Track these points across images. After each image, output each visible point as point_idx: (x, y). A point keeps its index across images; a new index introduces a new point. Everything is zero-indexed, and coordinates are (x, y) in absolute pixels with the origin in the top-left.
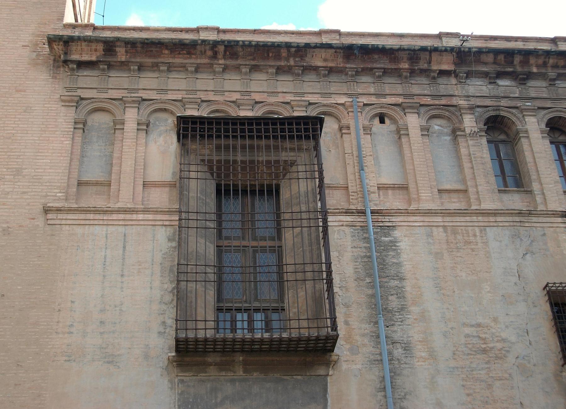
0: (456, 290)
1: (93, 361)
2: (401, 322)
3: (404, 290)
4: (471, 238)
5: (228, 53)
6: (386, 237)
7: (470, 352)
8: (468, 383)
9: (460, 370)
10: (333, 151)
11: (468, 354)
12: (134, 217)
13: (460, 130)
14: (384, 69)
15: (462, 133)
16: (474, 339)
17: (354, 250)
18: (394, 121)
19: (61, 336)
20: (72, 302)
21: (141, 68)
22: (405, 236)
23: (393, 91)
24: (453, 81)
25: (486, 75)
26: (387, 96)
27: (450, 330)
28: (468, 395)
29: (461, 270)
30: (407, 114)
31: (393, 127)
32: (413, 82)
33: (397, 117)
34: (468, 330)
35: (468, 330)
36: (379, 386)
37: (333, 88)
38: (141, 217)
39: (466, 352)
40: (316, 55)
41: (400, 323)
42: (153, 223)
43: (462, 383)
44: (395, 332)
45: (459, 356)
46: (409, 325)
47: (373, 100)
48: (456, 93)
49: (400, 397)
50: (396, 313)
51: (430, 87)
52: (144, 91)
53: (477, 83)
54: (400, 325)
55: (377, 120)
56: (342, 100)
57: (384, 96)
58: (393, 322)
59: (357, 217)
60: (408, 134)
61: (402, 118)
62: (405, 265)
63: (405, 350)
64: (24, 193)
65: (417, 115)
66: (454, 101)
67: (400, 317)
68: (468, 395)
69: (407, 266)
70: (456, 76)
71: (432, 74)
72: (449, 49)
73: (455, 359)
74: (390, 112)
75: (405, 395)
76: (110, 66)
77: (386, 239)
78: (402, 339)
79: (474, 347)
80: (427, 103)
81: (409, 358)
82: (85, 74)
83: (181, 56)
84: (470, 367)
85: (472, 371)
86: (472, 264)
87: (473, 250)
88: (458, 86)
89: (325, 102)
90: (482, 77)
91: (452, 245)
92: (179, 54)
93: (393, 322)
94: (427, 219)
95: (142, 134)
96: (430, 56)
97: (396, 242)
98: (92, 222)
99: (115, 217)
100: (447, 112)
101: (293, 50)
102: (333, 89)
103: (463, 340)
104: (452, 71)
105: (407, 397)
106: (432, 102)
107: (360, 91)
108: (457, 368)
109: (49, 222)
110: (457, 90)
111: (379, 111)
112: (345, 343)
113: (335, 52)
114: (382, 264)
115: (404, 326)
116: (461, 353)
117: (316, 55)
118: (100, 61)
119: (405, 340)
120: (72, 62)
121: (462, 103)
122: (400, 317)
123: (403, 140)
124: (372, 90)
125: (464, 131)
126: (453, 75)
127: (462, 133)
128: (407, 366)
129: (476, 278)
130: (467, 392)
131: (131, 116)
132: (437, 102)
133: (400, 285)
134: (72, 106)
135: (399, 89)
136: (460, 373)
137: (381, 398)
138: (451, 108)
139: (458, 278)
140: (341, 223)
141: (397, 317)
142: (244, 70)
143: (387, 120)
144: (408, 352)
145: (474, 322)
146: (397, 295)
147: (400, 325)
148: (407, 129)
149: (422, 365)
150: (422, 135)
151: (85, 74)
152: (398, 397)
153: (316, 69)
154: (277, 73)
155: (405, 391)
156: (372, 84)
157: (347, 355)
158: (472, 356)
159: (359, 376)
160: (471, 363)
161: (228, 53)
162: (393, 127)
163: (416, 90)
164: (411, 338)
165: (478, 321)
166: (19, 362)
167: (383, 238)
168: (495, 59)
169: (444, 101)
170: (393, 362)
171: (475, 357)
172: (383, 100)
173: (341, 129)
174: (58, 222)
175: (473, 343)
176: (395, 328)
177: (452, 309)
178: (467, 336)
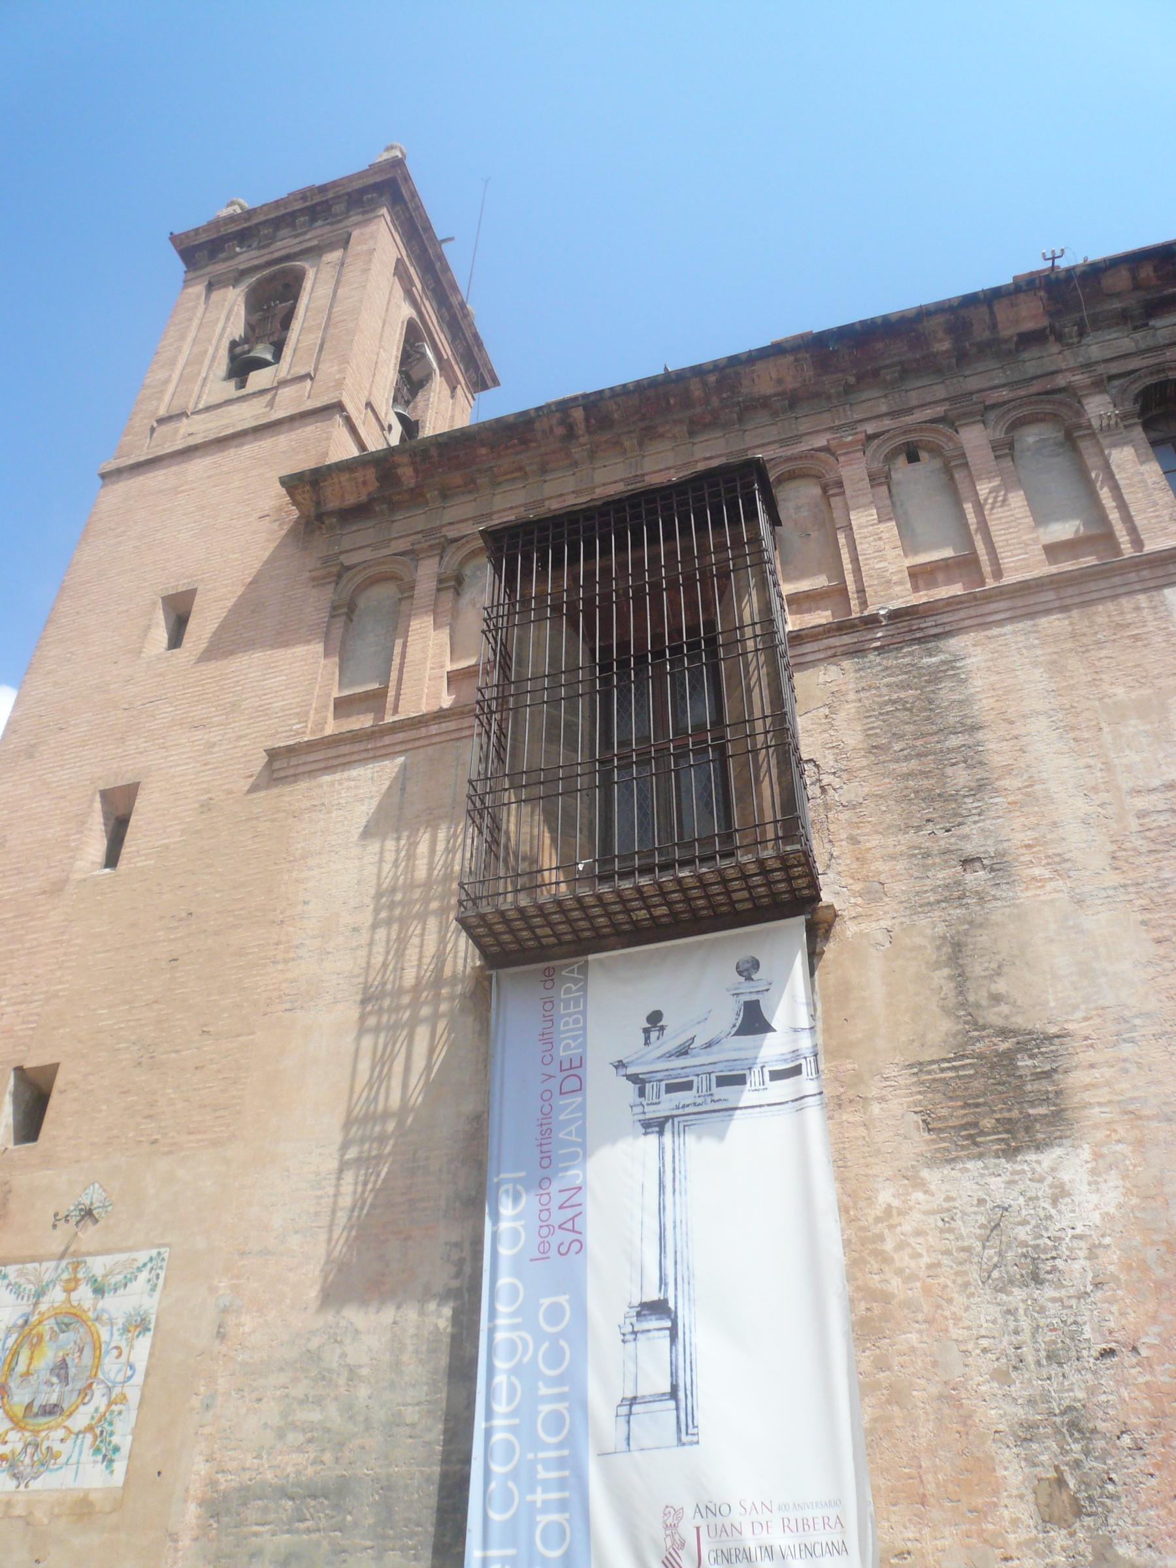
0: (1103, 725)
1: (335, 1003)
2: (980, 815)
3: (981, 748)
4: (1128, 616)
5: (593, 421)
6: (930, 656)
7: (1153, 847)
8: (1157, 916)
9: (1132, 889)
10: (814, 535)
11: (1150, 852)
12: (423, 732)
13: (1079, 427)
14: (901, 363)
15: (1087, 432)
16: (1162, 818)
17: (862, 695)
18: (936, 451)
19: (280, 967)
20: (305, 903)
21: (445, 494)
22: (974, 645)
23: (927, 399)
24: (1054, 348)
25: (1123, 318)
26: (915, 411)
27: (1100, 810)
28: (1159, 942)
29: (1112, 684)
30: (959, 430)
31: (937, 463)
32: (967, 373)
33: (941, 440)
34: (1141, 803)
35: (1141, 803)
36: (934, 957)
37: (804, 426)
38: (434, 729)
39: (1144, 849)
40: (758, 376)
41: (977, 818)
42: (456, 735)
43: (1140, 917)
44: (966, 837)
45: (1127, 861)
46: (999, 817)
47: (887, 423)
48: (1063, 366)
49: (987, 973)
50: (966, 800)
51: (1005, 373)
52: (451, 527)
53: (1108, 337)
54: (975, 822)
55: (902, 460)
56: (821, 441)
57: (909, 411)
58: (960, 819)
59: (864, 633)
60: (966, 464)
61: (950, 439)
62: (980, 700)
63: (992, 870)
64: (240, 738)
65: (982, 425)
66: (1061, 381)
67: (975, 805)
68: (1159, 942)
69: (984, 701)
70: (1059, 337)
71: (1004, 347)
72: (1023, 284)
73: (1117, 869)
74: (926, 437)
75: (999, 967)
76: (394, 507)
77: (933, 660)
78: (982, 849)
79: (1161, 835)
80: (1001, 400)
81: (1004, 887)
82: (354, 528)
83: (510, 451)
84: (1157, 879)
85: (1165, 886)
86: (1138, 666)
87: (1136, 638)
88: (1066, 352)
89: (789, 453)
90: (1118, 324)
91: (1085, 640)
92: (507, 448)
93: (960, 819)
94: (1019, 602)
95: (449, 595)
96: (992, 313)
97: (954, 661)
98: (348, 759)
99: (387, 740)
100: (1057, 409)
101: (712, 379)
102: (803, 429)
103: (1134, 824)
104: (1045, 329)
105: (1005, 969)
106: (1012, 395)
107: (857, 417)
108: (1124, 886)
109: (275, 776)
110: (1068, 360)
111: (901, 440)
112: (851, 881)
113: (796, 360)
114: (926, 710)
115: (988, 822)
116: (1131, 853)
117: (758, 376)
118: (375, 499)
119: (992, 851)
120: (331, 514)
121: (1079, 379)
122: (975, 805)
123: (956, 476)
124: (884, 409)
125: (1090, 426)
126: (1052, 338)
127: (1087, 432)
128: (999, 904)
129: (1150, 691)
130: (1157, 934)
131: (427, 573)
132: (1022, 393)
133: (970, 742)
134: (329, 583)
135: (940, 392)
136: (1132, 896)
137: (942, 981)
138: (1057, 396)
139: (1106, 700)
140: (830, 653)
141: (970, 806)
142: (627, 444)
143: (923, 455)
144: (1000, 873)
145: (1156, 783)
146: (965, 762)
147: (975, 822)
148: (963, 455)
149: (1036, 895)
150: (997, 457)
151: (354, 528)
152: (983, 974)
153: (763, 403)
154: (692, 433)
155: (999, 957)
156: (883, 400)
157: (856, 904)
158: (1160, 856)
159: (888, 945)
160: (1159, 869)
161: (593, 421)
162: (937, 463)
163: (973, 383)
164: (1006, 844)
165: (1165, 778)
166: (205, 1025)
167: (925, 660)
168: (1134, 278)
169: (1036, 387)
170: (964, 901)
171: (1167, 854)
172: (908, 419)
173: (825, 489)
174: (291, 771)
175: (1160, 827)
176: (965, 830)
177: (1100, 766)
178: (1142, 814)
